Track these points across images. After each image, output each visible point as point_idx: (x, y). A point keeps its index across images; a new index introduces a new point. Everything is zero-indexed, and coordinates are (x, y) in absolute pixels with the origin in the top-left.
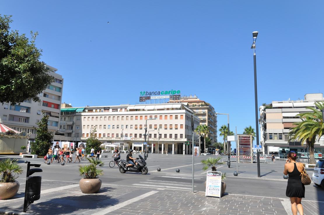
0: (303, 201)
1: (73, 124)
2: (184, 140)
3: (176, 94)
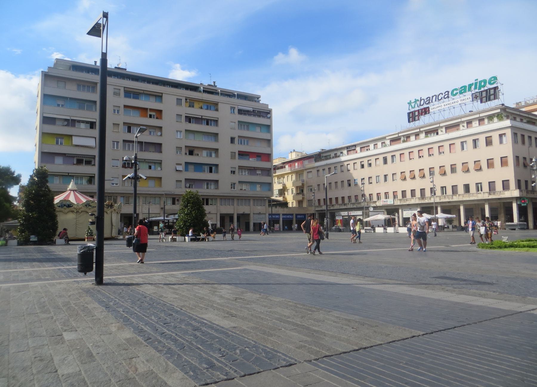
0: (106, 279)
1: (303, 184)
2: (514, 192)
3: (488, 86)
